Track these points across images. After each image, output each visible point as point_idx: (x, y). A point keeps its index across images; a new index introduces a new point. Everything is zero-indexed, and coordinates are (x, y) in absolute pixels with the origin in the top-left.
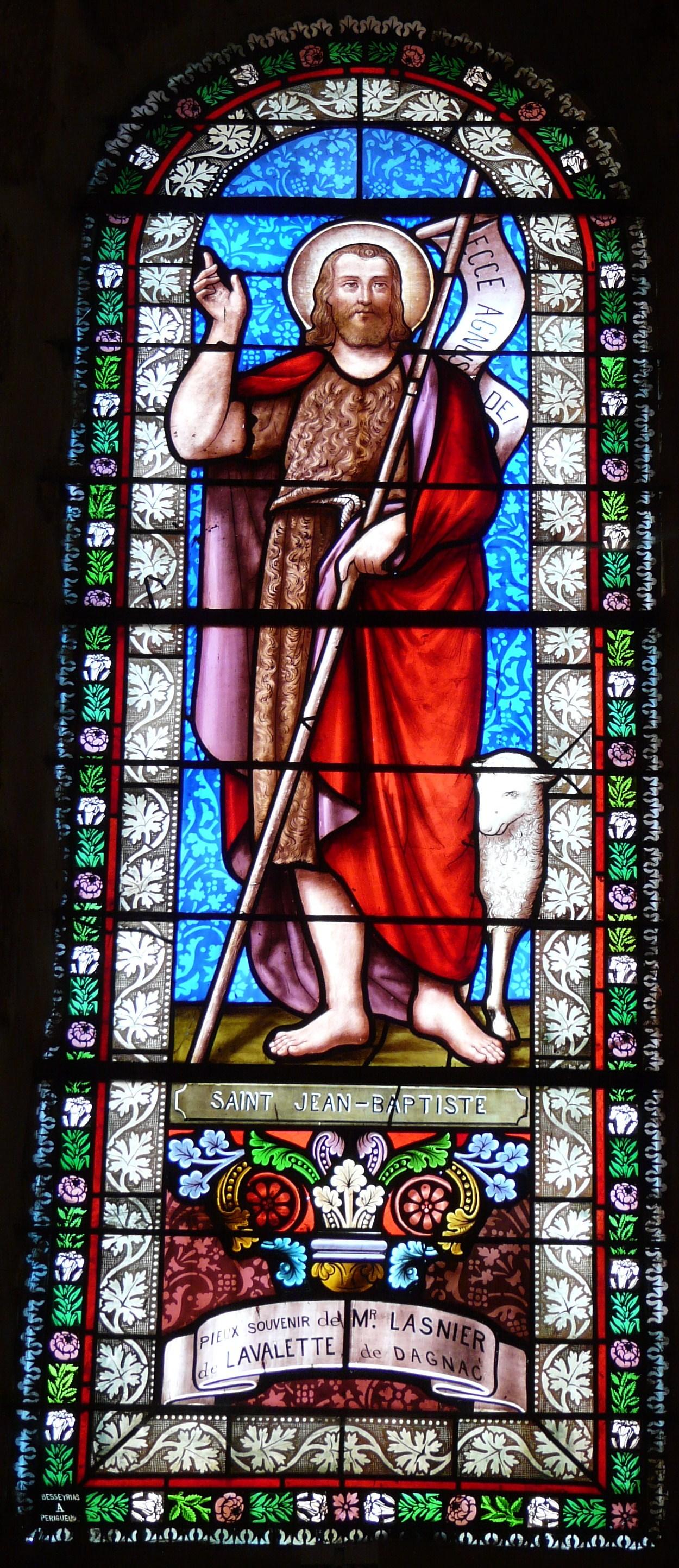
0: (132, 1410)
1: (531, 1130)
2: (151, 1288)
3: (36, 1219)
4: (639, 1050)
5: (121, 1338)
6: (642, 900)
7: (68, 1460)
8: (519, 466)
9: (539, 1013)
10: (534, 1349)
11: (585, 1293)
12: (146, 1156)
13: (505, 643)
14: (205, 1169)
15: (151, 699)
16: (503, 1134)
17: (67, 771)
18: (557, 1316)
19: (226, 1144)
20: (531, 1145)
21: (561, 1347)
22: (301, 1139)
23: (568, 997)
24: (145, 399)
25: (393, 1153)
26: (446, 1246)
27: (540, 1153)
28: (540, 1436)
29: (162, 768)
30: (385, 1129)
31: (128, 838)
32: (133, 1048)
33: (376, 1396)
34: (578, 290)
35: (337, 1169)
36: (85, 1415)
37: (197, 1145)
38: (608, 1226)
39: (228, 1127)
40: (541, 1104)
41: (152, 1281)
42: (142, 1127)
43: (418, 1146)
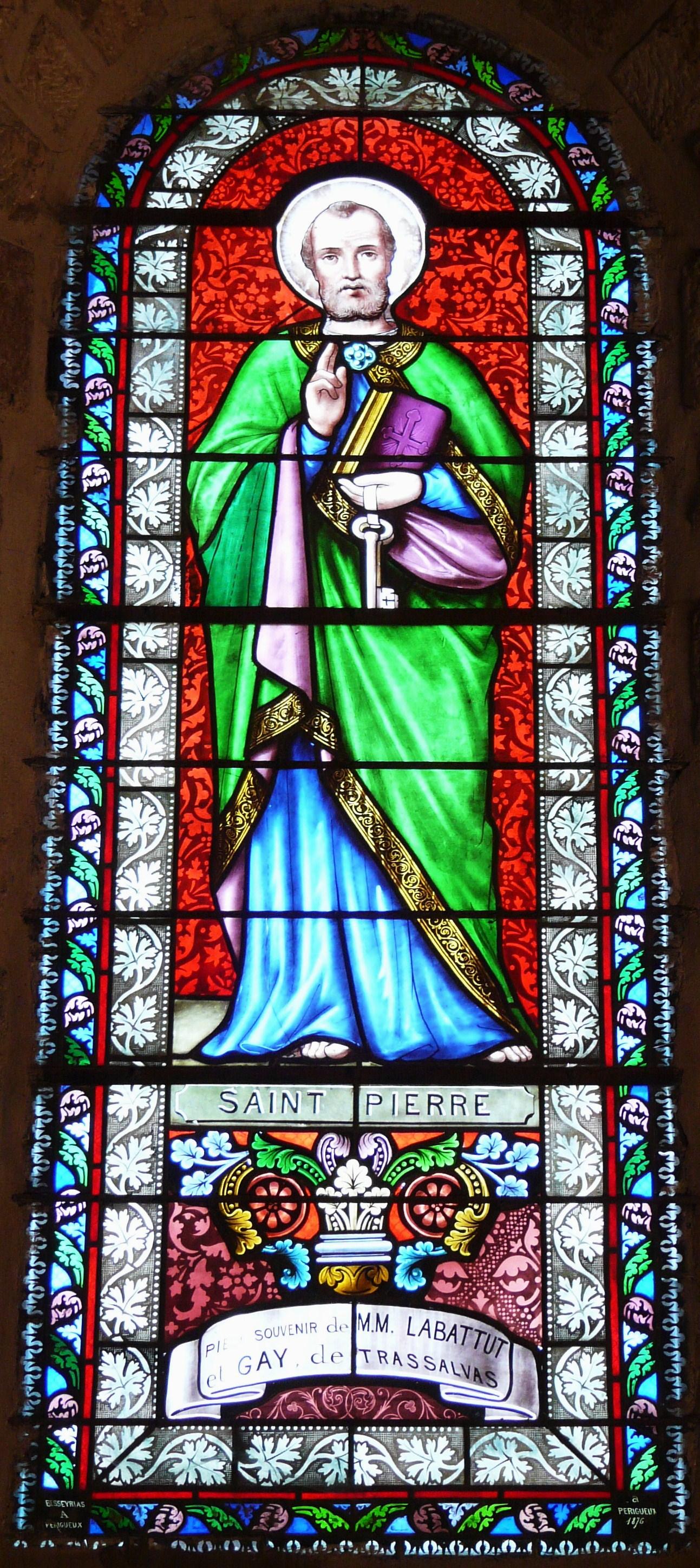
1: (540, 1129)
10: (545, 1208)
11: (595, 1151)
12: (142, 1304)
14: (209, 1170)
15: (146, 704)
16: (511, 1134)
18: (564, 1037)
19: (229, 1146)
20: (542, 1145)
22: (306, 1140)
23: (576, 998)
24: (111, 1325)
25: (397, 1153)
27: (544, 750)
28: (553, 1440)
31: (109, 1257)
34: (579, 389)
35: (341, 1170)
42: (142, 1131)
43: (427, 1144)
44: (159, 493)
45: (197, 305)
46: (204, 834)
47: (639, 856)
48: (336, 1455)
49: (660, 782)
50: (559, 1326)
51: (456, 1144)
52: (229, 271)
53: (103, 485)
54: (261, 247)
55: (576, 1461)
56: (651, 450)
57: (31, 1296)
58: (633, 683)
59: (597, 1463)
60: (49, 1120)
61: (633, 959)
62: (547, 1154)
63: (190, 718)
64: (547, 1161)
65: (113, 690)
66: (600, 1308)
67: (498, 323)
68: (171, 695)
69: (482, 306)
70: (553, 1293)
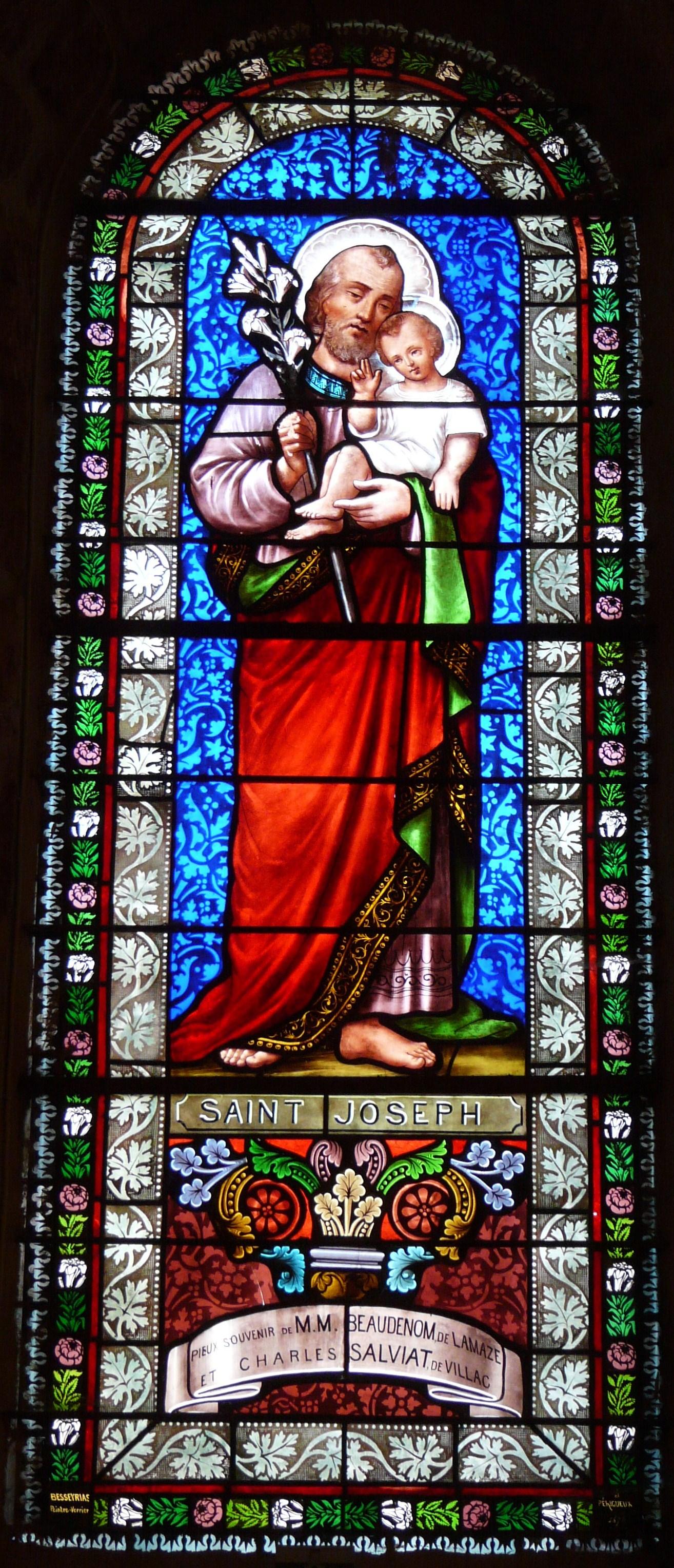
0: (135, 1416)
1: (528, 1137)
2: (153, 1296)
3: (66, 389)
4: (624, 476)
5: (133, 930)
6: (634, 896)
7: (101, 565)
8: (513, 864)
9: (533, 887)
12: (146, 1164)
16: (500, 1142)
18: (551, 1041)
19: (227, 1153)
20: (528, 1154)
21: (558, 1217)
25: (391, 1160)
26: (443, 1251)
28: (536, 1440)
29: (166, 405)
33: (379, 1403)
37: (198, 1153)
38: (606, 1229)
40: (537, 1115)
41: (154, 1289)
44: (145, 881)
46: (192, 1283)
48: (331, 1451)
52: (211, 844)
56: (644, 737)
57: (41, 1160)
63: (186, 759)
67: (493, 895)
70: (534, 887)
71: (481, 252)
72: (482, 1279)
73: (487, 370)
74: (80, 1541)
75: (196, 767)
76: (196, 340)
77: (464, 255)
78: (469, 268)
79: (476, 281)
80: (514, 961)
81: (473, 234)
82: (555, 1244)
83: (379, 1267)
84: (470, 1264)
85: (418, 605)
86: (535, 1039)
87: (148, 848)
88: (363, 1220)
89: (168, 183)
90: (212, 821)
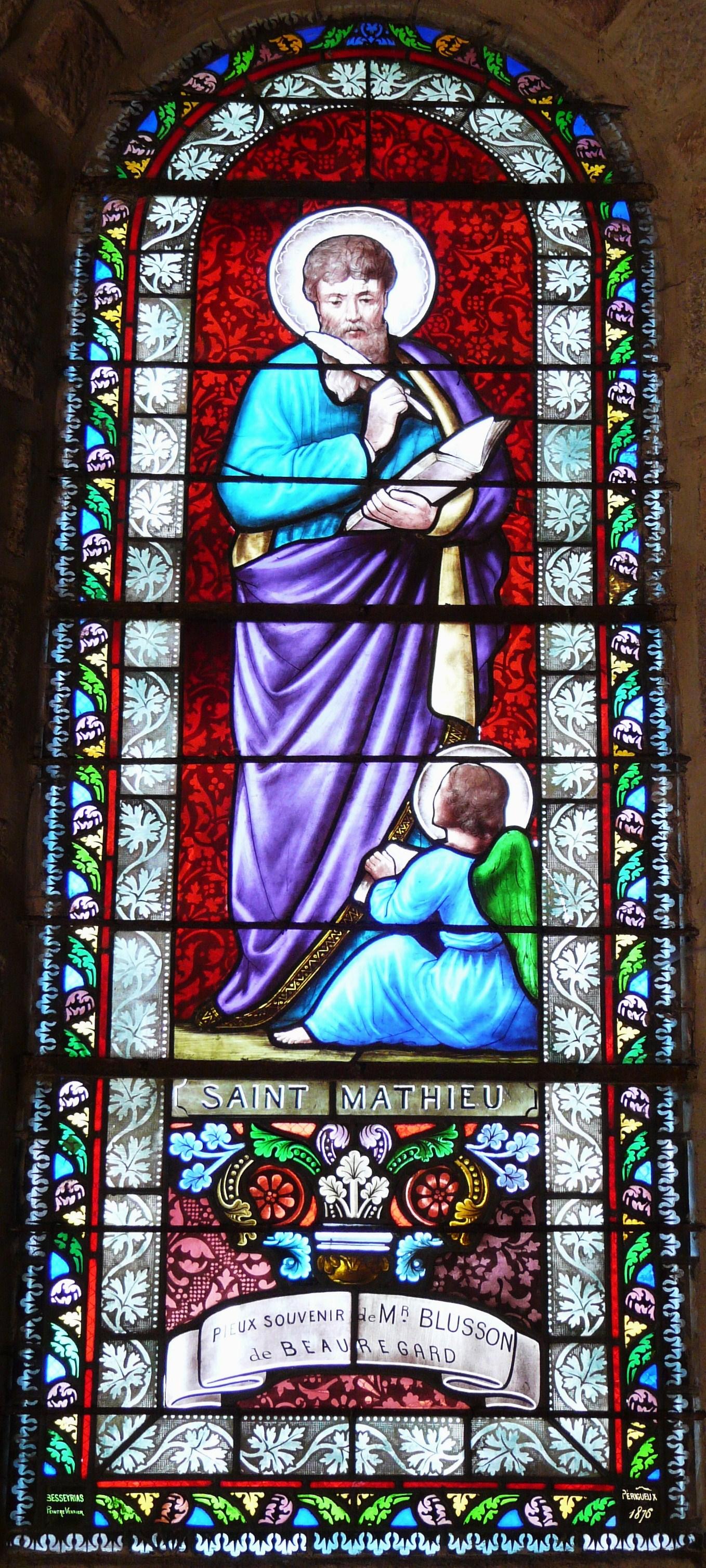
8: (523, 452)
12: (142, 1295)
13: (504, 394)
16: (513, 1125)
17: (79, 373)
18: (569, 1314)
19: (228, 1138)
27: (550, 1154)
28: (554, 1433)
30: (390, 1122)
32: (154, 412)
34: (584, 515)
36: (129, 356)
37: (198, 1138)
39: (228, 1120)
45: (197, 388)
47: (632, 415)
48: (339, 1445)
49: (658, 538)
50: (548, 407)
51: (455, 1135)
52: (229, 353)
53: (101, 645)
54: (261, 328)
55: (576, 1454)
58: (631, 422)
59: (598, 1457)
60: (62, 833)
61: (632, 858)
62: (547, 1144)
64: (547, 1151)
65: (117, 698)
66: (597, 1168)
67: (509, 727)
68: (180, 449)
69: (489, 237)
70: (548, 887)
71: (497, 308)
72: (492, 228)
73: (503, 671)
74: (76, 1543)
75: (201, 749)
76: (205, 322)
77: (479, 310)
78: (484, 324)
79: (491, 337)
80: (524, 314)
81: (488, 291)
82: (570, 1228)
83: (387, 1248)
84: (481, 215)
85: (429, 658)
86: (552, 1312)
87: (155, 717)
88: (370, 1203)
89: (178, 166)
90: (229, 333)
